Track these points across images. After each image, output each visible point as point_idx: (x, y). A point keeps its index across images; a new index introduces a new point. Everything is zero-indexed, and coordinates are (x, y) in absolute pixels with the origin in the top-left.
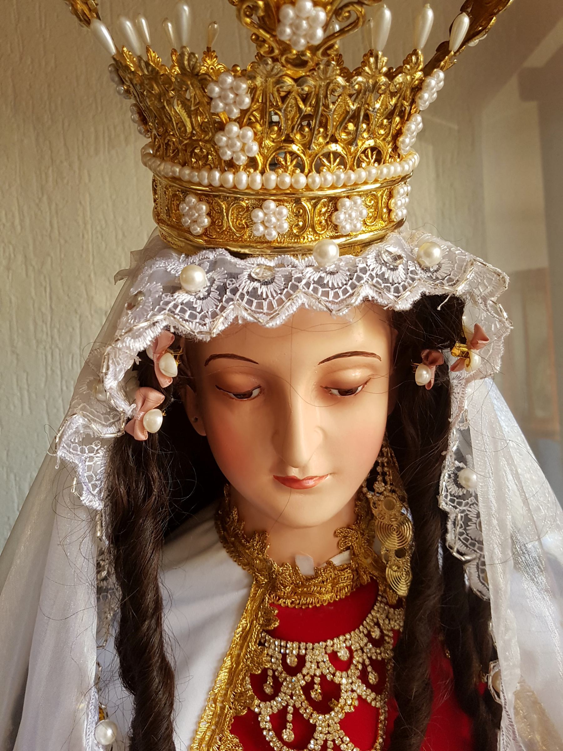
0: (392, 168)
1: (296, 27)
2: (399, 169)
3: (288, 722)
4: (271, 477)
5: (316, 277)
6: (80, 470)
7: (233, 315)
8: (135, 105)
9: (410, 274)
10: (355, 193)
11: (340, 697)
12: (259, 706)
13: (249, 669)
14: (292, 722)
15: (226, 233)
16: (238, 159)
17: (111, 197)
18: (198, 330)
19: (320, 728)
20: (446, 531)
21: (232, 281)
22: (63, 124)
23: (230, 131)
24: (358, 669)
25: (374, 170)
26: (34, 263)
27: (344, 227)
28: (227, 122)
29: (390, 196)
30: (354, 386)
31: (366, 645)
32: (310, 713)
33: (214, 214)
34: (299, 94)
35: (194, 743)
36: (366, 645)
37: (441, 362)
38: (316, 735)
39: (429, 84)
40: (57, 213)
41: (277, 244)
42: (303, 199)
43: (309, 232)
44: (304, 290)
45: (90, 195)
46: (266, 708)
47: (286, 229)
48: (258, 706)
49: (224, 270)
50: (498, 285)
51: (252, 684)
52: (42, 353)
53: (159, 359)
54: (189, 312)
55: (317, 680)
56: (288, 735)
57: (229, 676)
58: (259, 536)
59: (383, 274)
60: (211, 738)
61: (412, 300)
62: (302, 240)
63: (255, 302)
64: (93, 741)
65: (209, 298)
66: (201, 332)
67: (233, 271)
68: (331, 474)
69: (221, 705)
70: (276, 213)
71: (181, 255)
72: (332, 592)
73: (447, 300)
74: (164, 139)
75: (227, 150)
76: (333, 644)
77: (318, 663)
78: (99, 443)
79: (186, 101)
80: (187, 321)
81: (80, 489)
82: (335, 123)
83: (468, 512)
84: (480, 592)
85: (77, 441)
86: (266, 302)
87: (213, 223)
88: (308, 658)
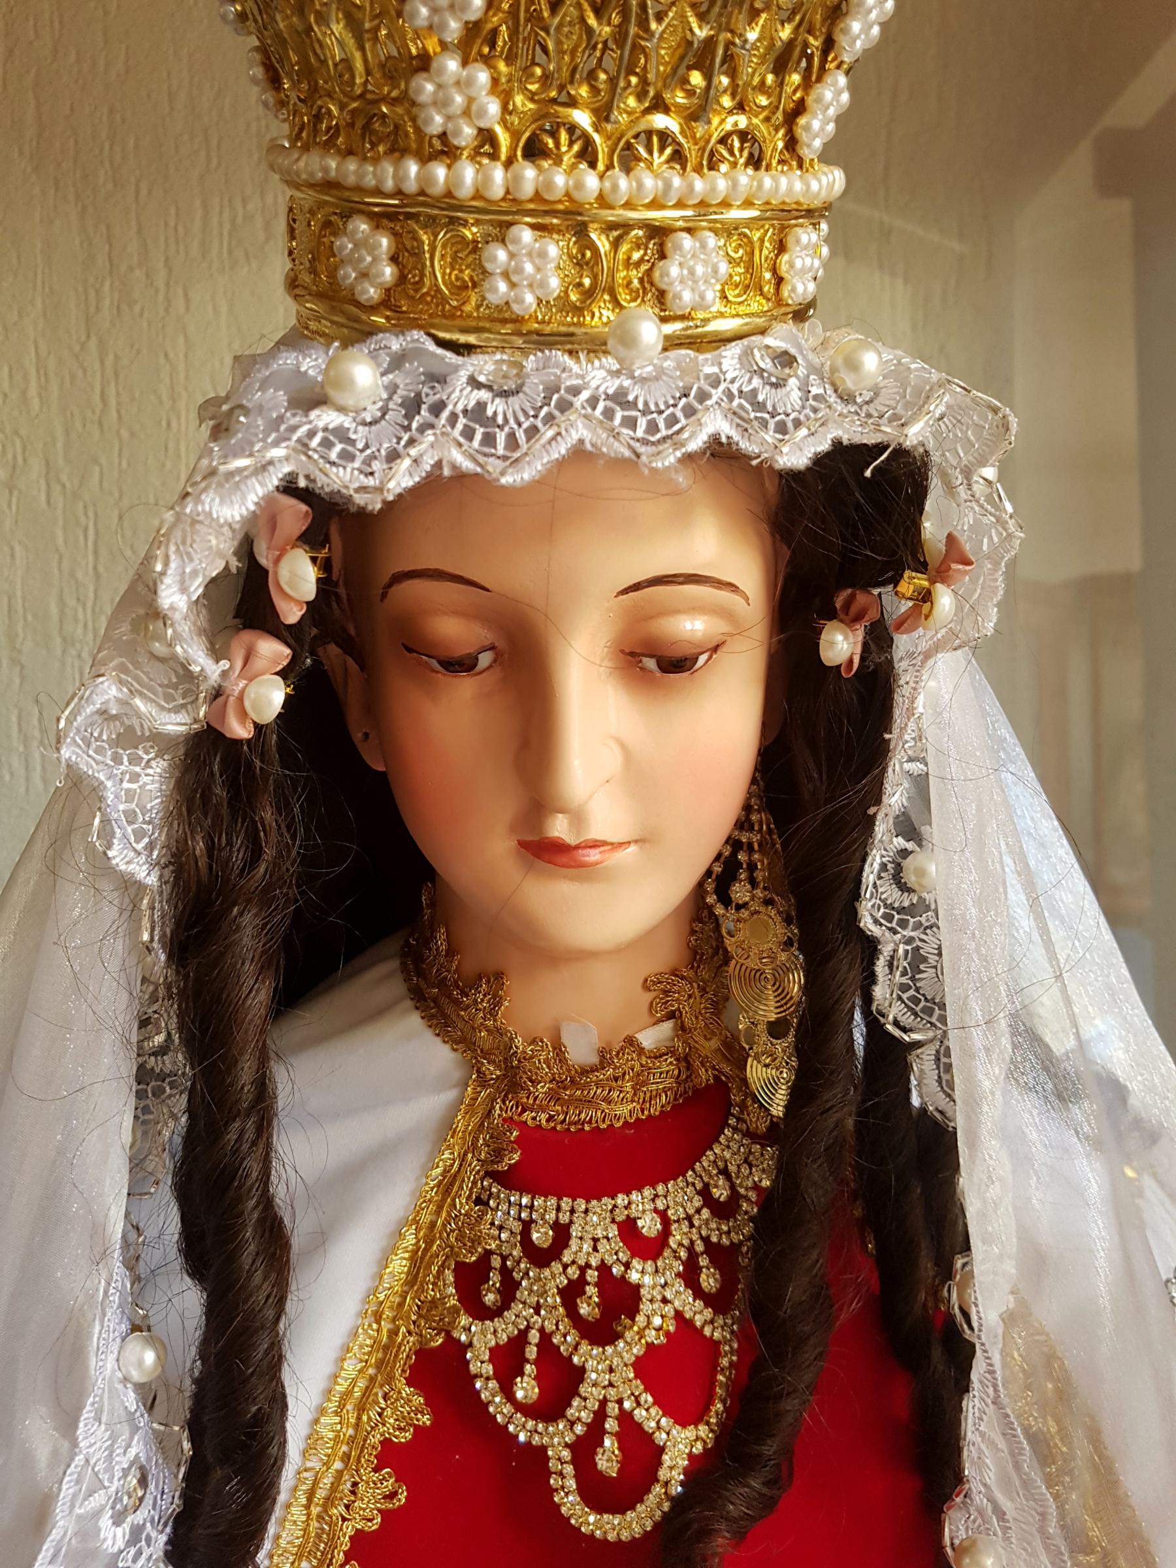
0: (784, 181)
2: (798, 186)
3: (528, 1361)
5: (612, 386)
6: (110, 797)
7: (432, 457)
8: (257, 49)
9: (811, 402)
10: (704, 224)
11: (637, 1311)
12: (468, 1330)
13: (453, 1253)
14: (536, 1362)
15: (429, 299)
16: (458, 132)
17: (230, 345)
18: (356, 485)
19: (594, 1376)
20: (871, 979)
21: (433, 388)
22: (138, 192)
23: (442, 71)
24: (679, 1258)
25: (745, 177)
26: (64, 478)
27: (678, 296)
28: (435, 54)
29: (781, 248)
30: (689, 651)
31: (698, 1211)
32: (574, 1343)
33: (405, 257)
35: (329, 1400)
36: (698, 1211)
37: (873, 615)
38: (583, 1389)
40: (116, 374)
41: (536, 325)
42: (592, 226)
43: (605, 302)
44: (583, 412)
46: (483, 1333)
47: (554, 291)
48: (467, 1328)
49: (418, 368)
50: (994, 439)
51: (458, 1285)
52: (73, 666)
53: (277, 561)
54: (339, 447)
55: (592, 1275)
56: (526, 1389)
57: (410, 1268)
58: (488, 981)
59: (754, 392)
60: (367, 1391)
61: (813, 450)
62: (588, 318)
63: (480, 432)
64: (113, 1371)
65: (383, 422)
66: (365, 488)
67: (437, 369)
68: (636, 841)
69: (390, 1326)
70: (534, 255)
71: (332, 342)
72: (632, 1101)
74: (312, 106)
75: (434, 113)
76: (630, 1203)
77: (595, 1240)
78: (152, 747)
79: (354, 11)
80: (333, 464)
81: (107, 834)
82: (662, 68)
83: (920, 944)
84: (941, 1112)
85: (105, 737)
86: (503, 434)
87: (402, 279)
88: (575, 1231)
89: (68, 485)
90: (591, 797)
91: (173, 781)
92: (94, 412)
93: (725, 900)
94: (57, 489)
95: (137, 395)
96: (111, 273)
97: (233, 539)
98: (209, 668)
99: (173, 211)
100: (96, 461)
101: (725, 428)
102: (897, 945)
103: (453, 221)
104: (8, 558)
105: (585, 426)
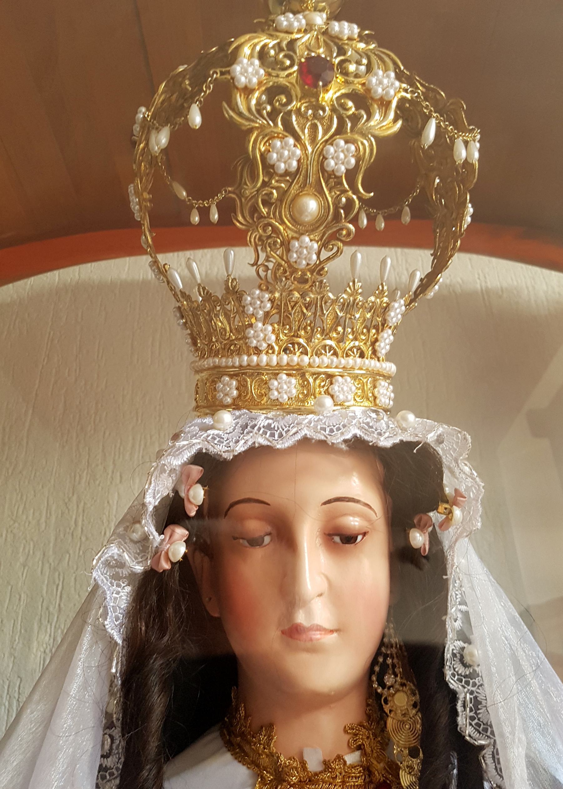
1: (299, 253)
4: (279, 633)
8: (189, 334)
16: (261, 346)
20: (455, 713)
22: (104, 433)
23: (256, 326)
25: (359, 360)
26: (51, 560)
33: (242, 389)
34: (303, 303)
39: (393, 306)
45: (118, 494)
58: (266, 729)
62: (306, 404)
73: (420, 445)
81: (105, 615)
87: (239, 396)
89: (52, 564)
90: (313, 599)
91: (132, 598)
92: (70, 529)
93: (383, 685)
94: (47, 565)
95: (92, 520)
96: (88, 468)
97: (173, 483)
98: (156, 538)
99: (119, 441)
100: (68, 552)
101: (359, 433)
102: (466, 695)
103: (259, 374)
104: (17, 600)
105: (307, 429)
